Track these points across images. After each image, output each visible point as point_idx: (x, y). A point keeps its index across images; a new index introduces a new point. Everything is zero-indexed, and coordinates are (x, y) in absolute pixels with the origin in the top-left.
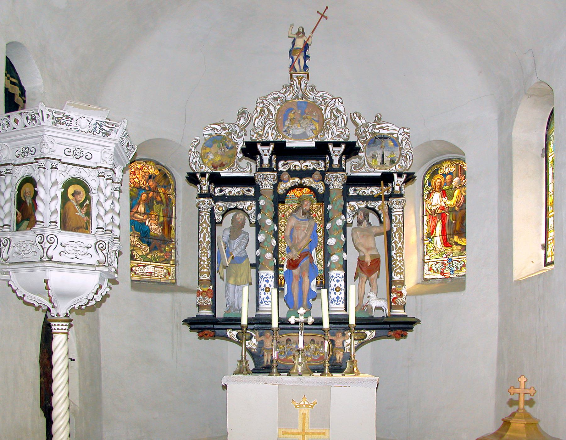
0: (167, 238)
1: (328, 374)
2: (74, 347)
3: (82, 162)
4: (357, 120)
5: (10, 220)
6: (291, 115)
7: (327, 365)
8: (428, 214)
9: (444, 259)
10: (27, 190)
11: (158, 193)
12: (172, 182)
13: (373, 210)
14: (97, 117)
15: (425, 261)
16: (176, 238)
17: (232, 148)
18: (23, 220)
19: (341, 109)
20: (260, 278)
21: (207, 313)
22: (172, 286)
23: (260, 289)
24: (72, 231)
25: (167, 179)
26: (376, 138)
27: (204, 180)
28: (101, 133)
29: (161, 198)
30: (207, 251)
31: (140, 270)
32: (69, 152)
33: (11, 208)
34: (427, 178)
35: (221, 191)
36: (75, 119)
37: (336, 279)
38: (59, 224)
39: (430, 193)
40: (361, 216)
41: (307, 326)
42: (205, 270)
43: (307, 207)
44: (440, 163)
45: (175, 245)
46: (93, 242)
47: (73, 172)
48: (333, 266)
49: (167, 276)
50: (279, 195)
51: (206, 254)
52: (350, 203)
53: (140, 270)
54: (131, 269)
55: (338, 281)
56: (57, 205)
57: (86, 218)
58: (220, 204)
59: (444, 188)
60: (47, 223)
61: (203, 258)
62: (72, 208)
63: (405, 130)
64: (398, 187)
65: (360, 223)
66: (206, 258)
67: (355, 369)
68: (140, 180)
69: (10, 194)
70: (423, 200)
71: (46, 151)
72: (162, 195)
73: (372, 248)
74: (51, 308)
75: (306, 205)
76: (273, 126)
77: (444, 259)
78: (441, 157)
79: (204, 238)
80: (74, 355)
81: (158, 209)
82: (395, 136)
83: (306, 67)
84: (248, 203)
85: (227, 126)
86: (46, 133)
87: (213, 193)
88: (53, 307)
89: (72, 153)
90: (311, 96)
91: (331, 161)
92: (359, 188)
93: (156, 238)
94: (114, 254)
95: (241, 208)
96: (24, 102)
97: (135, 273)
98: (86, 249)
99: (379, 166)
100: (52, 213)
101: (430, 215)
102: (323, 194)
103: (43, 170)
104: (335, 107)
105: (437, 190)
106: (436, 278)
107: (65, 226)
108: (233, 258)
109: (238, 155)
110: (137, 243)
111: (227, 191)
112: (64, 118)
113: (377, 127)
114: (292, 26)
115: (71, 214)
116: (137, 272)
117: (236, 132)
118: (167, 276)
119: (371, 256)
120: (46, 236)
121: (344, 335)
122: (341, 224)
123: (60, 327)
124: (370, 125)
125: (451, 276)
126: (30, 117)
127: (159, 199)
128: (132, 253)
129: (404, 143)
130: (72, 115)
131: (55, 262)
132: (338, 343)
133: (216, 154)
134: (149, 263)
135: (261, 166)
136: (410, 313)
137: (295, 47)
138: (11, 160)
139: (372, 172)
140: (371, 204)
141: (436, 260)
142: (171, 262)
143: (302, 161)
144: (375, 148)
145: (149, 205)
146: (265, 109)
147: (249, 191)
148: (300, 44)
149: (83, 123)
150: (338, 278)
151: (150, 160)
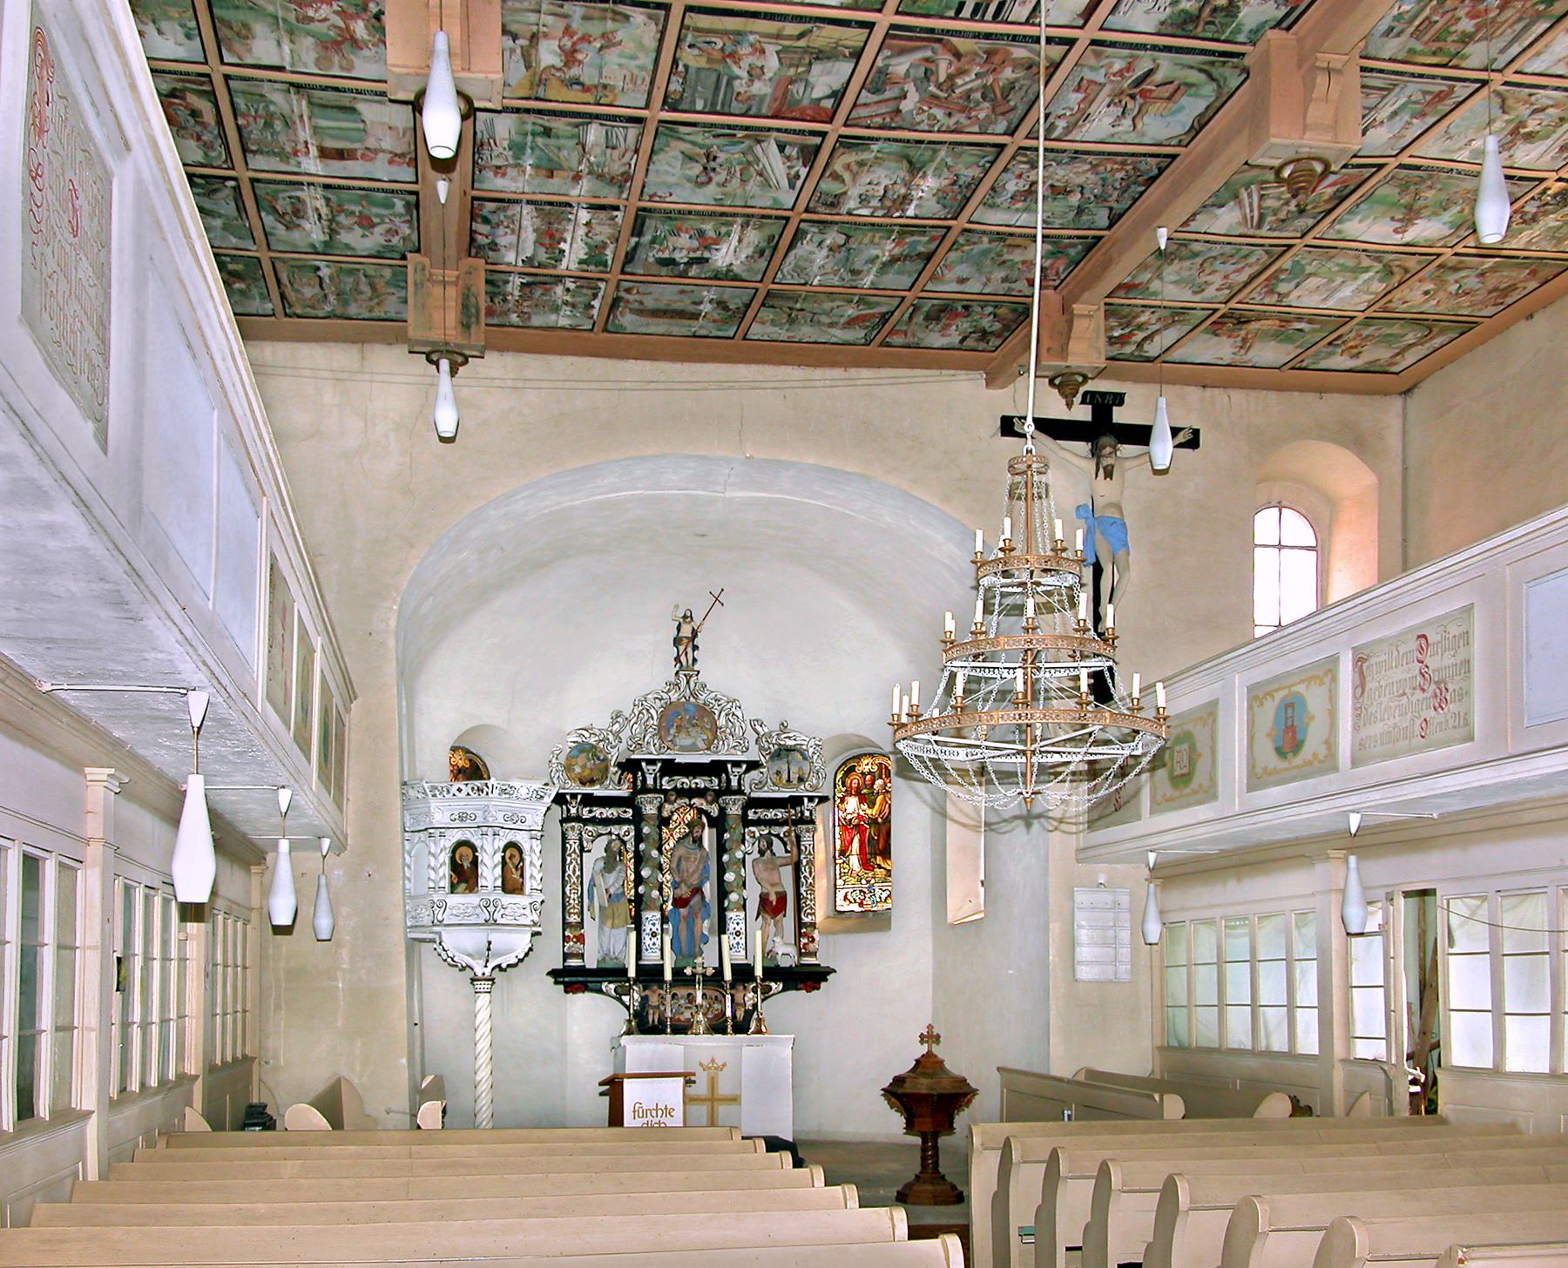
4: (758, 728)
5: (445, 883)
7: (730, 1023)
13: (777, 836)
19: (739, 713)
35: (590, 812)
44: (859, 757)
48: (731, 906)
58: (590, 828)
65: (762, 853)
83: (695, 660)
84: (625, 828)
85: (598, 732)
111: (598, 812)
114: (677, 606)
115: (508, 876)
119: (777, 893)
121: (745, 988)
132: (739, 997)
136: (821, 960)
140: (776, 830)
148: (686, 631)
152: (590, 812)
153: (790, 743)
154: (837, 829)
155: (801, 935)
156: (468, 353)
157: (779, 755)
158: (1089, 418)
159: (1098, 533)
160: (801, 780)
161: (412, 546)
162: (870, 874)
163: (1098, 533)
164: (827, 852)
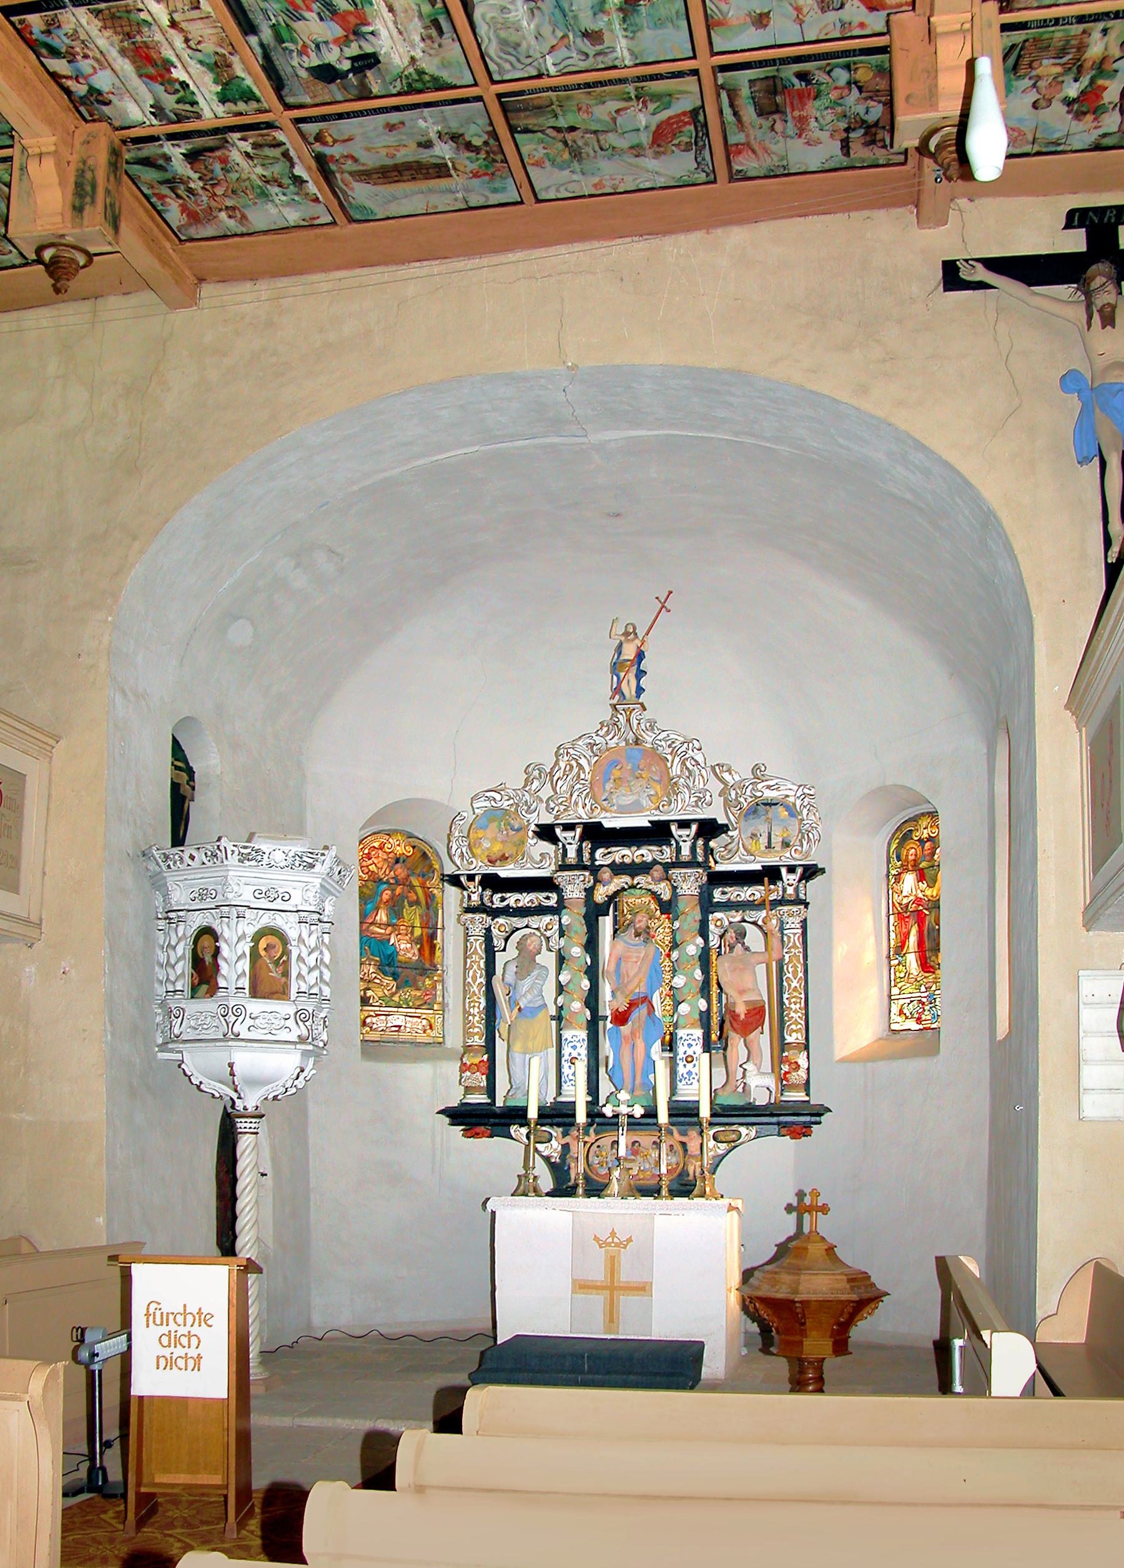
0: (427, 966)
1: (665, 1197)
2: (266, 1153)
3: (278, 904)
4: (726, 776)
6: (616, 773)
8: (896, 912)
9: (923, 995)
10: (206, 944)
11: (412, 887)
12: (437, 867)
14: (296, 848)
15: (893, 998)
16: (445, 963)
17: (518, 830)
18: (200, 984)
19: (699, 757)
20: (563, 1042)
21: (481, 1098)
22: (437, 1049)
23: (563, 1059)
24: (264, 998)
25: (428, 862)
26: (758, 805)
27: (472, 886)
28: (302, 867)
29: (416, 894)
30: (479, 998)
31: (379, 1023)
32: (259, 894)
33: (184, 967)
34: (894, 846)
35: (503, 899)
36: (267, 853)
37: (686, 1043)
38: (247, 991)
39: (900, 874)
40: (732, 937)
41: (631, 1120)
42: (476, 1030)
43: (643, 925)
45: (440, 976)
46: (292, 1013)
47: (266, 920)
48: (681, 1022)
49: (429, 1031)
50: (597, 904)
51: (477, 1004)
52: (715, 914)
53: (379, 1023)
54: (364, 1024)
55: (690, 1045)
56: (245, 965)
57: (284, 979)
58: (501, 920)
59: (921, 866)
60: (232, 990)
61: (472, 1010)
62: (264, 967)
63: (806, 791)
64: (792, 888)
66: (476, 1010)
67: (708, 1189)
68: (378, 866)
69: (183, 949)
70: (888, 885)
71: (230, 896)
72: (419, 890)
73: (749, 989)
74: (235, 1099)
75: (640, 921)
76: (585, 793)
77: (923, 995)
78: (916, 808)
79: (474, 979)
80: (267, 1168)
81: (413, 916)
82: (792, 799)
86: (231, 873)
87: (490, 904)
88: (239, 1098)
89: (263, 895)
90: (648, 737)
91: (679, 849)
92: (730, 889)
93: (406, 965)
94: (322, 1022)
95: (536, 927)
96: (193, 788)
97: (371, 1028)
98: (283, 1021)
99: (763, 852)
100: (239, 977)
101: (899, 913)
102: (670, 900)
103: (227, 920)
104: (687, 756)
105: (910, 868)
106: (909, 1030)
107: (255, 993)
108: (520, 1009)
109: (530, 841)
110: (374, 975)
111: (513, 899)
112: (253, 853)
113: (760, 786)
116: (375, 1026)
117: (526, 802)
118: (429, 1031)
120: (231, 1007)
122: (693, 953)
123: (245, 1125)
124: (747, 784)
125: (933, 1026)
126: (209, 853)
127: (413, 897)
128: (365, 993)
129: (805, 812)
130: (264, 848)
131: (243, 1040)
133: (494, 840)
134: (396, 1009)
135: (563, 860)
137: (622, 658)
138: (184, 905)
139: (751, 862)
140: (752, 915)
141: (910, 995)
142: (436, 1007)
143: (634, 848)
144: (757, 821)
145: (395, 907)
146: (574, 763)
147: (548, 898)
148: (629, 652)
149: (278, 856)
150: (690, 1041)
151: (396, 832)
152: (503, 899)
153: (770, 794)
154: (892, 917)
155: (782, 1060)
156: (93, 250)
157: (755, 812)
158: (1084, 249)
159: (1098, 410)
160: (786, 844)
161: (135, 538)
162: (931, 978)
163: (1098, 410)
164: (879, 952)
